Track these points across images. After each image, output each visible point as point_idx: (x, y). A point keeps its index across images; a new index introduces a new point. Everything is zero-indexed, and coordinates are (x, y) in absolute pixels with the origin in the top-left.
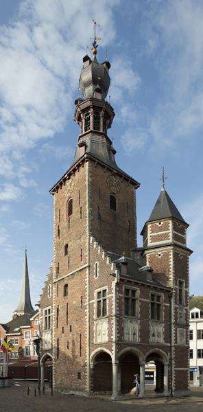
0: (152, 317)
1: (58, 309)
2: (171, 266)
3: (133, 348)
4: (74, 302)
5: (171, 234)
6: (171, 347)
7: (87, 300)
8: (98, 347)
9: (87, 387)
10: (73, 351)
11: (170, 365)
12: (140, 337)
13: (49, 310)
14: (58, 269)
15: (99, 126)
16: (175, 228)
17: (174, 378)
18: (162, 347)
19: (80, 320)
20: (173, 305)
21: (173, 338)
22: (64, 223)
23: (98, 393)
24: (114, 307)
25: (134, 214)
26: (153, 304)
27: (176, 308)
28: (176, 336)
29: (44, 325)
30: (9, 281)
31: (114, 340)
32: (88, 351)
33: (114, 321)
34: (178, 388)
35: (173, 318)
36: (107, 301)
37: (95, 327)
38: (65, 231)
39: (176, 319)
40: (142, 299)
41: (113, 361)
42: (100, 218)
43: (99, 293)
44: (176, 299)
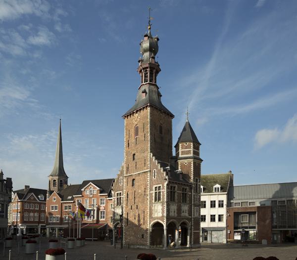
0: (183, 202)
2: (192, 170)
4: (140, 191)
5: (192, 151)
6: (191, 218)
7: (149, 191)
8: (155, 219)
9: (149, 243)
10: (139, 221)
11: (191, 229)
12: (177, 213)
14: (128, 168)
15: (184, 154)
16: (194, 147)
17: (193, 237)
18: (187, 219)
19: (143, 201)
22: (133, 140)
24: (165, 197)
25: (171, 135)
27: (194, 195)
28: (194, 212)
29: (116, 202)
30: (31, 137)
31: (165, 216)
32: (149, 222)
33: (165, 205)
35: (193, 201)
36: (162, 193)
38: (133, 145)
39: (194, 202)
41: (165, 227)
42: (155, 141)
43: (156, 188)
44: (194, 190)
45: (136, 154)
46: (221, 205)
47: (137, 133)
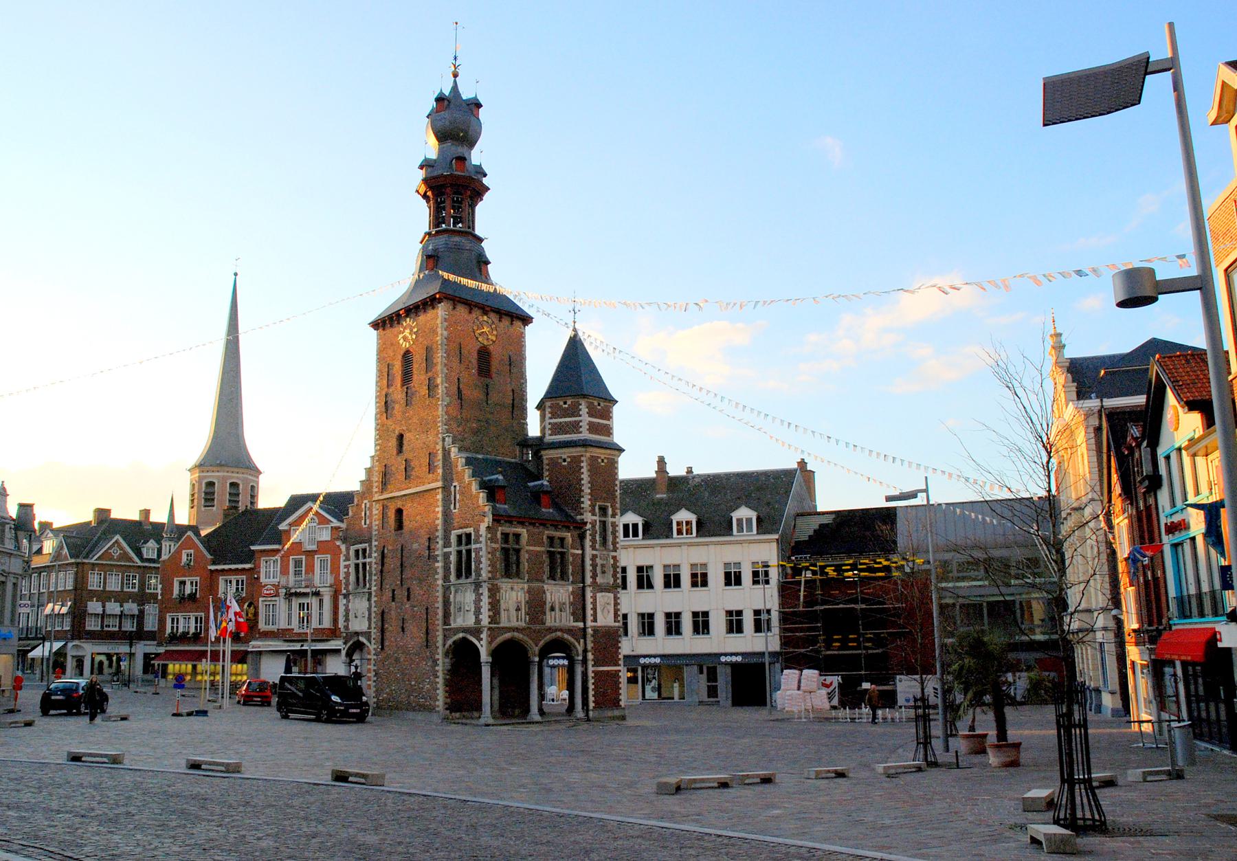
1: (383, 552)
3: (516, 634)
4: (415, 546)
6: (585, 629)
11: (585, 661)
13: (364, 550)
15: (559, 433)
18: (570, 631)
20: (589, 552)
21: (589, 612)
23: (458, 715)
26: (551, 555)
27: (594, 557)
29: (352, 578)
34: (598, 705)
35: (588, 575)
36: (473, 555)
37: (452, 596)
39: (594, 576)
40: (531, 548)
42: (460, 397)
44: (593, 541)
45: (407, 436)
46: (759, 577)
47: (407, 376)
